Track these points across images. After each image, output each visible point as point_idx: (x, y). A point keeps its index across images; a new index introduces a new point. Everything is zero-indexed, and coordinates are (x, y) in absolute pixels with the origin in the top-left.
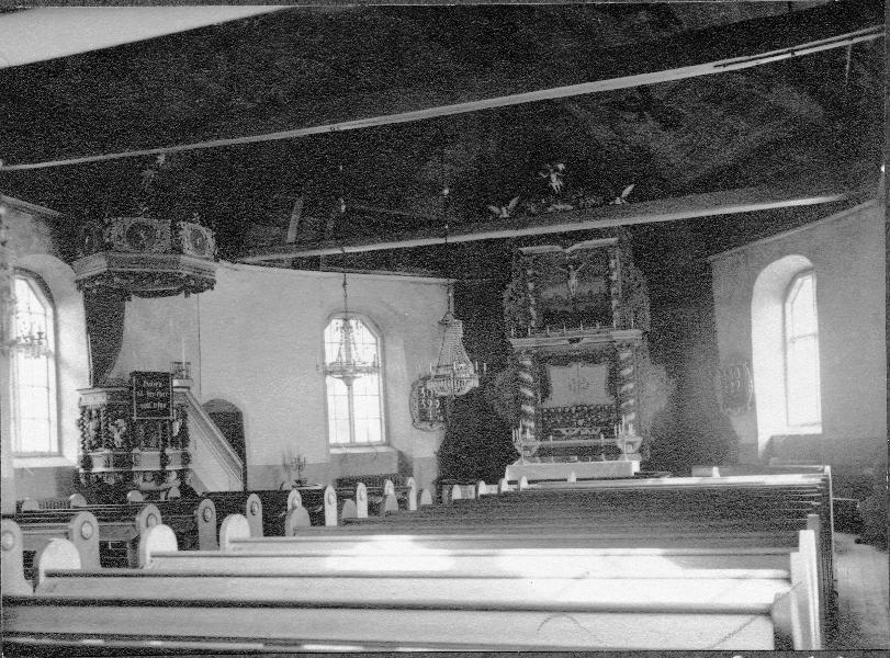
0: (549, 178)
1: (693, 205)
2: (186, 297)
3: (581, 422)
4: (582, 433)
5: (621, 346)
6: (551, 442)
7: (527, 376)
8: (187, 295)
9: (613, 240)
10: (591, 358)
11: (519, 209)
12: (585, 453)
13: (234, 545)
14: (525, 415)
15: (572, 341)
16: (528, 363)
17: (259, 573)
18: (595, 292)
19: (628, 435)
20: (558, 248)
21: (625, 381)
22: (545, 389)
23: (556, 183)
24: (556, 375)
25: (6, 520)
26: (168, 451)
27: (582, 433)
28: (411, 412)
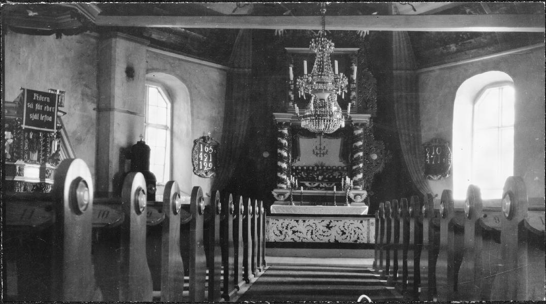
2: (57, 38)
3: (320, 178)
7: (284, 142)
13: (100, 217)
16: (286, 131)
21: (357, 149)
22: (295, 151)
24: (305, 144)
25: (228, 13)
26: (48, 165)
27: (321, 186)
28: (193, 162)
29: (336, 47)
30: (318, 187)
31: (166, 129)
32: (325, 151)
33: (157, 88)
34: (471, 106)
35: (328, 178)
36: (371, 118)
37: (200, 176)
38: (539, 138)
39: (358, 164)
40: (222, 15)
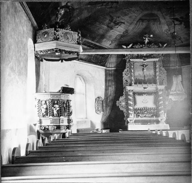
0: (145, 39)
1: (118, 51)
3: (146, 112)
4: (146, 116)
5: (160, 90)
6: (139, 118)
7: (131, 98)
8: (62, 61)
9: (157, 59)
10: (149, 93)
11: (132, 47)
12: (150, 122)
14: (130, 110)
15: (144, 88)
17: (159, 177)
18: (151, 74)
19: (163, 117)
20: (142, 60)
21: (160, 100)
23: (147, 41)
24: (138, 98)
27: (146, 116)
29: (125, 59)
30: (145, 116)
31: (83, 95)
32: (147, 101)
33: (80, 78)
34: (142, 72)
35: (149, 113)
36: (165, 87)
37: (98, 114)
38: (2, 48)
39: (162, 106)
40: (106, 49)
